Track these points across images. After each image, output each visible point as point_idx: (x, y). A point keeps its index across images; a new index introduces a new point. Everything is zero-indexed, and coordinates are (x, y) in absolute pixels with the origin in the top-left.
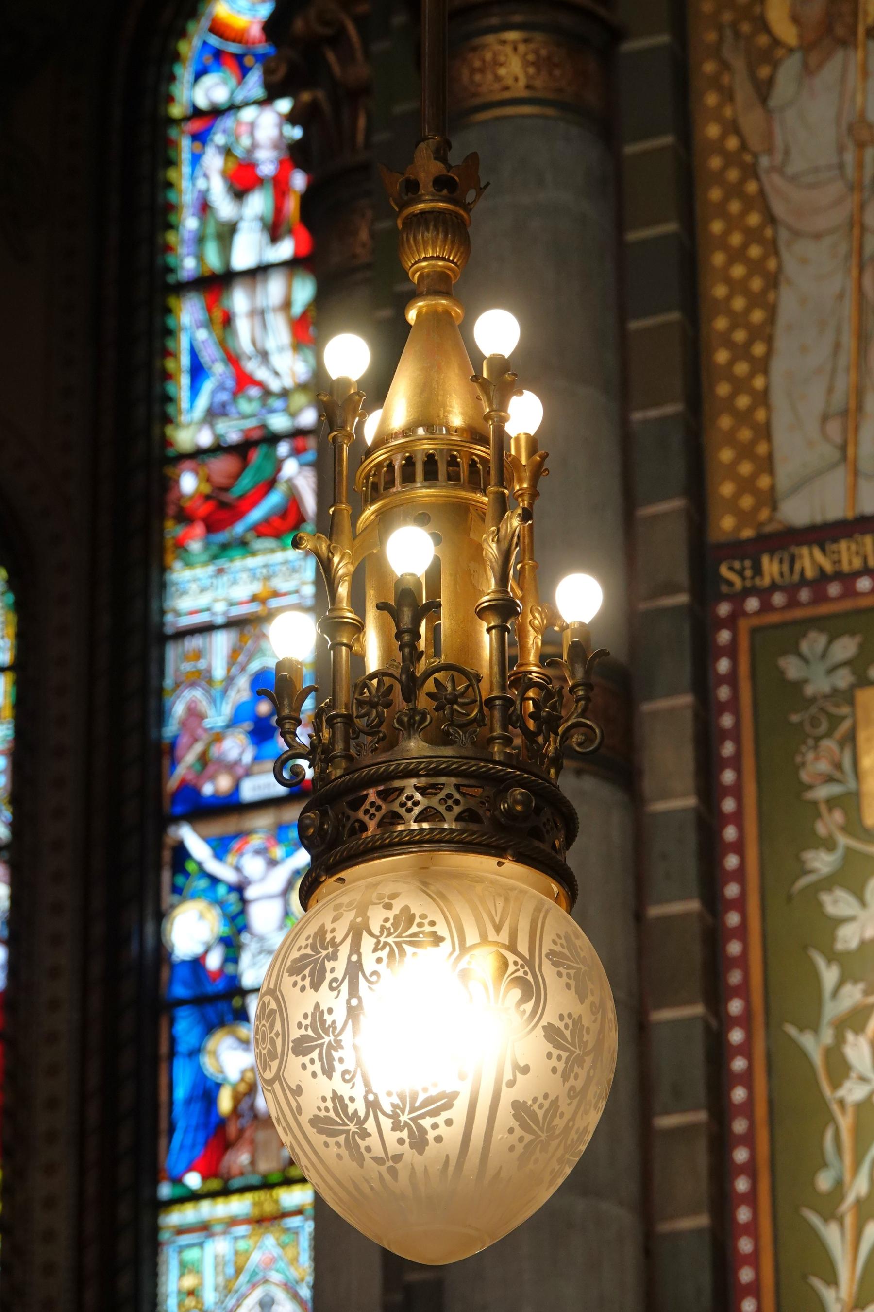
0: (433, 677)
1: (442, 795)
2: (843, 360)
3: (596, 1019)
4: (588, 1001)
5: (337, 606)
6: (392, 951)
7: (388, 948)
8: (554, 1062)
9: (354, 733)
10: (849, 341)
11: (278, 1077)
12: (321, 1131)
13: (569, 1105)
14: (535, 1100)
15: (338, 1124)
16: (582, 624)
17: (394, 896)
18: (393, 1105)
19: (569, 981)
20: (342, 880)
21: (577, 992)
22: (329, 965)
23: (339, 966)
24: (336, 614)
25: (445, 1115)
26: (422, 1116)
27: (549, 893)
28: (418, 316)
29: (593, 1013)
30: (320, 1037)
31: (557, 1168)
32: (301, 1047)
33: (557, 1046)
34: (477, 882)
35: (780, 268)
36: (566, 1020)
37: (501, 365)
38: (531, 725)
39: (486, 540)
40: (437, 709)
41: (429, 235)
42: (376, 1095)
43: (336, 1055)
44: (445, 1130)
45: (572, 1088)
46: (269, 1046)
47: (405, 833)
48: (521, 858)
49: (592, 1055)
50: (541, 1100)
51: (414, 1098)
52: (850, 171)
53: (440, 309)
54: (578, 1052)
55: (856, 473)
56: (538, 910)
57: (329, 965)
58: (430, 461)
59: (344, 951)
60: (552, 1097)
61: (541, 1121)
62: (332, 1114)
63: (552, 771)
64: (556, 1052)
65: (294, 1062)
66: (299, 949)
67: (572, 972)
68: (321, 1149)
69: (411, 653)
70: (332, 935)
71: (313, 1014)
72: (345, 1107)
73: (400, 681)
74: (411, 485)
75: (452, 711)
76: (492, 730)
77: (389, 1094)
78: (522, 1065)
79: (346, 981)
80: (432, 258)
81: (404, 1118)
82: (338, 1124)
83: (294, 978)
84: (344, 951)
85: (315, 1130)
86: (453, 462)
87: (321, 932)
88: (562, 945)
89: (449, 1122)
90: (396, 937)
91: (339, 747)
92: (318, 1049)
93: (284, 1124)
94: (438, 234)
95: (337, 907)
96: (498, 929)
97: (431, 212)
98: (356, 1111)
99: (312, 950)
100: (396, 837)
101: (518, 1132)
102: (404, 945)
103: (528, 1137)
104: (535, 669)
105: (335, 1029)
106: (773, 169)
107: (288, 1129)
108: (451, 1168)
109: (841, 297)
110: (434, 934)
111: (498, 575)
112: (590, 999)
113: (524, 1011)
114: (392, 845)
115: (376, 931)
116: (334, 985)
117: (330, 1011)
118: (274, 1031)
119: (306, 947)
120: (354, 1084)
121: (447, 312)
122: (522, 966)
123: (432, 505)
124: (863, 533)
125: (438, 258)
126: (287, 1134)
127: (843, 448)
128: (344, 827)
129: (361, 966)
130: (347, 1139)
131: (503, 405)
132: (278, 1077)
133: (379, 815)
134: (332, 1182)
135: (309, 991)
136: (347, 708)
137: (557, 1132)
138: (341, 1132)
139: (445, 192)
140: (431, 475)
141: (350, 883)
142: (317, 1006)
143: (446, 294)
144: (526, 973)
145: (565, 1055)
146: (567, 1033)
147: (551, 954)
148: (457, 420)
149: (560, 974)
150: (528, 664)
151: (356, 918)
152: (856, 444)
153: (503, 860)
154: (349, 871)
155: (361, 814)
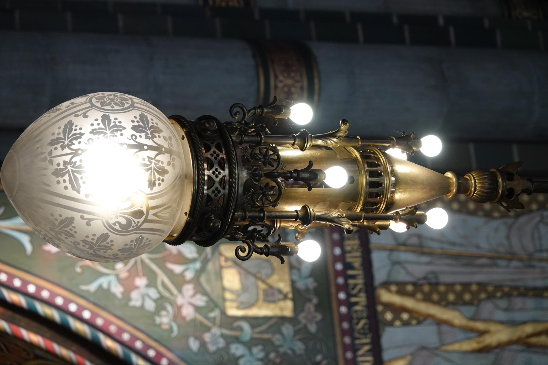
0: (276, 185)
1: (220, 188)
2: (446, 246)
5: (313, 140)
9: (253, 146)
10: (456, 250)
12: (66, 126)
14: (74, 227)
15: (68, 135)
16: (297, 252)
17: (174, 166)
18: (76, 162)
20: (183, 138)
22: (143, 135)
23: (142, 140)
24: (309, 139)
25: (69, 186)
26: (69, 176)
27: (173, 232)
28: (449, 178)
29: (113, 255)
30: (110, 129)
32: (106, 119)
33: (99, 239)
35: (495, 218)
36: (110, 243)
37: (421, 220)
38: (251, 228)
39: (339, 211)
40: (260, 187)
41: (486, 185)
42: (80, 155)
44: (62, 186)
45: (79, 244)
46: (108, 102)
48: (188, 223)
49: (93, 253)
50: (74, 230)
51: (78, 172)
52: (538, 255)
53: (451, 189)
54: (95, 247)
55: (392, 250)
56: (163, 231)
57: (143, 135)
58: (379, 184)
59: (150, 142)
60: (75, 235)
62: (73, 132)
63: (229, 236)
64: (96, 238)
65: (99, 115)
66: (152, 120)
67: (133, 247)
68: (57, 125)
69: (287, 177)
71: (120, 126)
72: (76, 139)
73: (274, 170)
74: (367, 174)
75: (259, 194)
76: (249, 212)
77: (81, 161)
78: (91, 223)
80: (476, 186)
81: (69, 167)
83: (138, 117)
84: (150, 142)
86: (378, 195)
87: (159, 131)
88: (146, 242)
89: (66, 188)
90: (154, 168)
91: (246, 138)
93: (71, 107)
94: (486, 189)
95: (170, 138)
96: (155, 215)
97: (498, 186)
98: (74, 144)
101: (60, 219)
103: (57, 223)
104: (278, 226)
106: (542, 217)
108: (45, 187)
109: (478, 247)
111: (323, 216)
114: (197, 160)
118: (114, 106)
119: (153, 123)
121: (449, 191)
123: (358, 184)
124: (363, 252)
125: (475, 189)
126: (66, 107)
127: (404, 244)
128: (208, 141)
129: (142, 150)
131: (402, 220)
132: (93, 106)
133: (212, 158)
134: (43, 128)
135: (132, 124)
136: (264, 142)
137: (59, 236)
138: (65, 136)
139: (506, 193)
140: (372, 185)
141: (181, 142)
142: (124, 128)
143: (459, 191)
144: (133, 227)
145: (94, 242)
146: (104, 243)
147: (142, 238)
148: (398, 196)
149: (132, 241)
150: (281, 222)
151: (165, 148)
152: (405, 251)
154: (187, 143)
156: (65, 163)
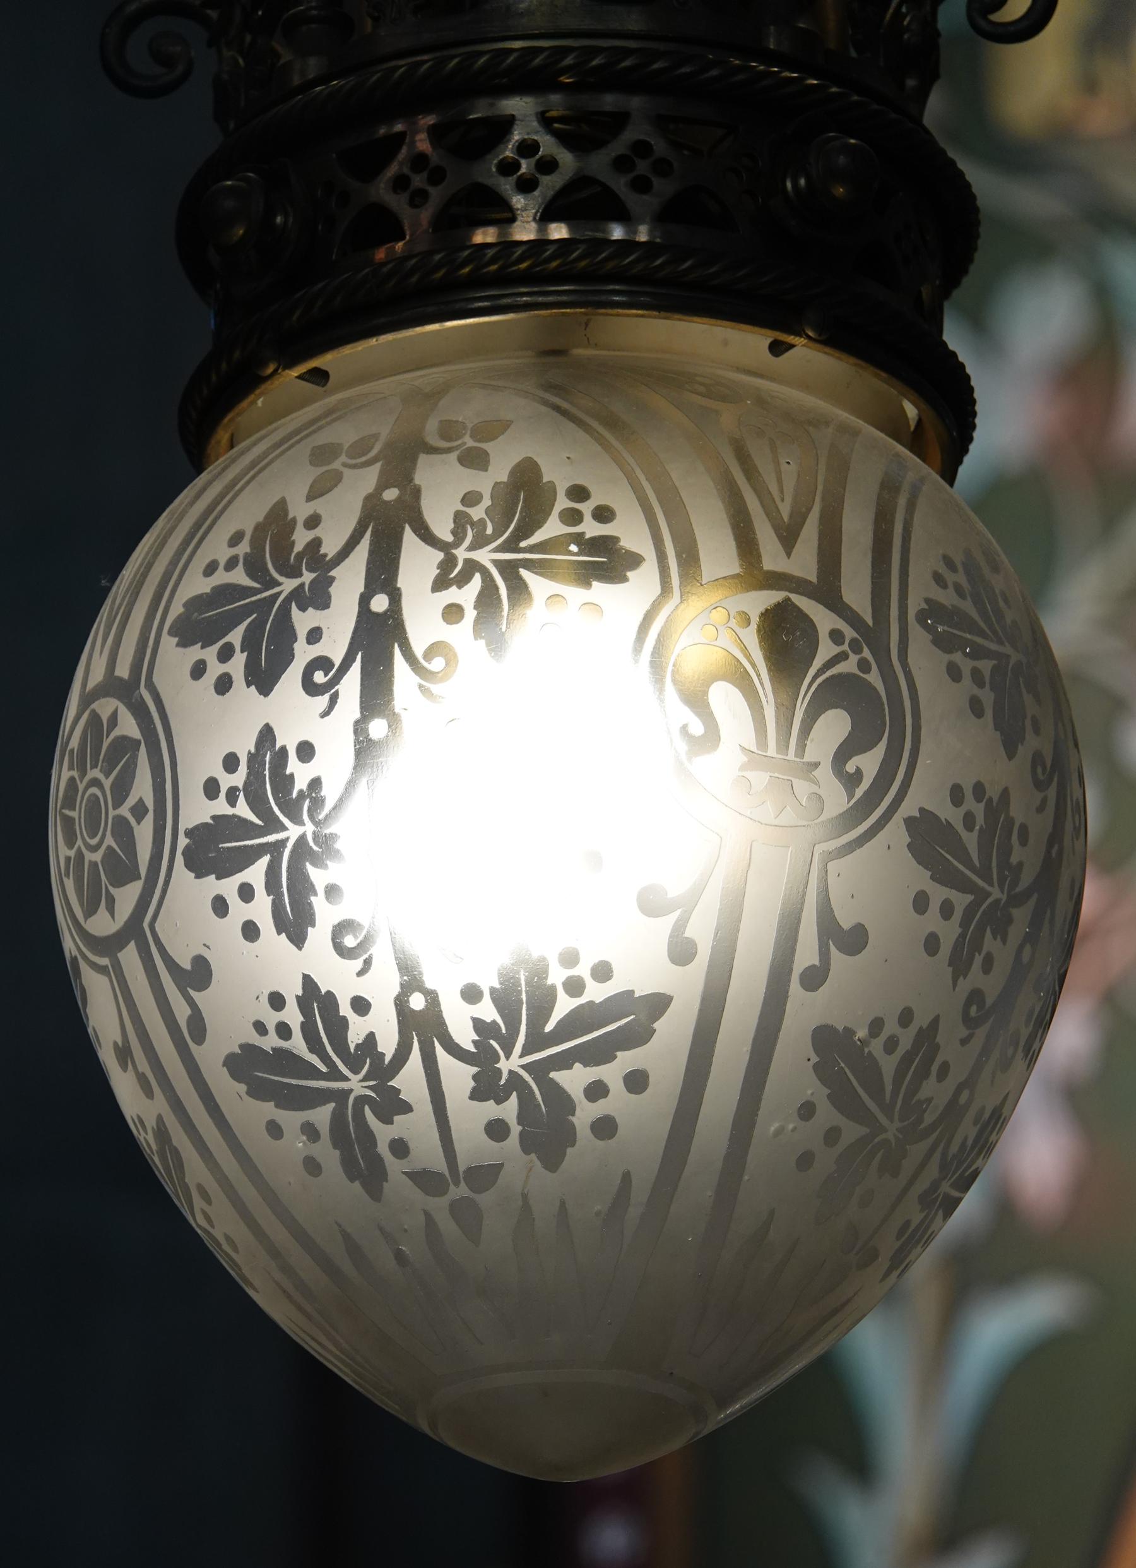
1: (619, 147)
3: (1044, 801)
4: (1024, 752)
6: (489, 587)
7: (477, 581)
8: (932, 921)
11: (135, 930)
12: (259, 1091)
13: (964, 1042)
14: (876, 1026)
17: (491, 430)
19: (976, 691)
20: (319, 377)
21: (997, 727)
22: (303, 620)
25: (626, 1060)
26: (564, 1061)
29: (1039, 785)
31: (917, 1218)
32: (215, 850)
33: (944, 876)
34: (724, 399)
42: (432, 998)
43: (318, 876)
45: (976, 996)
46: (109, 841)
47: (490, 253)
48: (835, 338)
49: (1032, 902)
50: (891, 1027)
54: (996, 893)
56: (889, 488)
57: (303, 620)
59: (349, 581)
60: (921, 1020)
61: (889, 1088)
62: (298, 1044)
64: (938, 893)
65: (190, 893)
66: (211, 569)
70: (310, 535)
72: (337, 1027)
77: (471, 994)
78: (846, 923)
79: (356, 668)
81: (511, 1064)
82: (315, 1073)
84: (349, 581)
85: (242, 1088)
87: (278, 524)
90: (506, 547)
92: (265, 860)
93: (144, 1066)
95: (323, 455)
96: (788, 538)
99: (251, 574)
100: (493, 260)
102: (523, 572)
103: (852, 1131)
105: (317, 803)
107: (156, 1079)
108: (634, 1213)
110: (603, 545)
112: (1031, 743)
113: (858, 775)
115: (444, 532)
116: (319, 677)
117: (306, 751)
118: (131, 801)
119: (231, 564)
120: (368, 963)
122: (855, 647)
126: (149, 1094)
130: (338, 1119)
132: (135, 930)
135: (243, 693)
137: (929, 1119)
138: (323, 1097)
144: (864, 666)
145: (960, 900)
146: (971, 840)
147: (932, 611)
149: (954, 673)
151: (382, 486)
153: (791, 339)
154: (348, 350)
155: (381, 190)
156: (487, 1087)
